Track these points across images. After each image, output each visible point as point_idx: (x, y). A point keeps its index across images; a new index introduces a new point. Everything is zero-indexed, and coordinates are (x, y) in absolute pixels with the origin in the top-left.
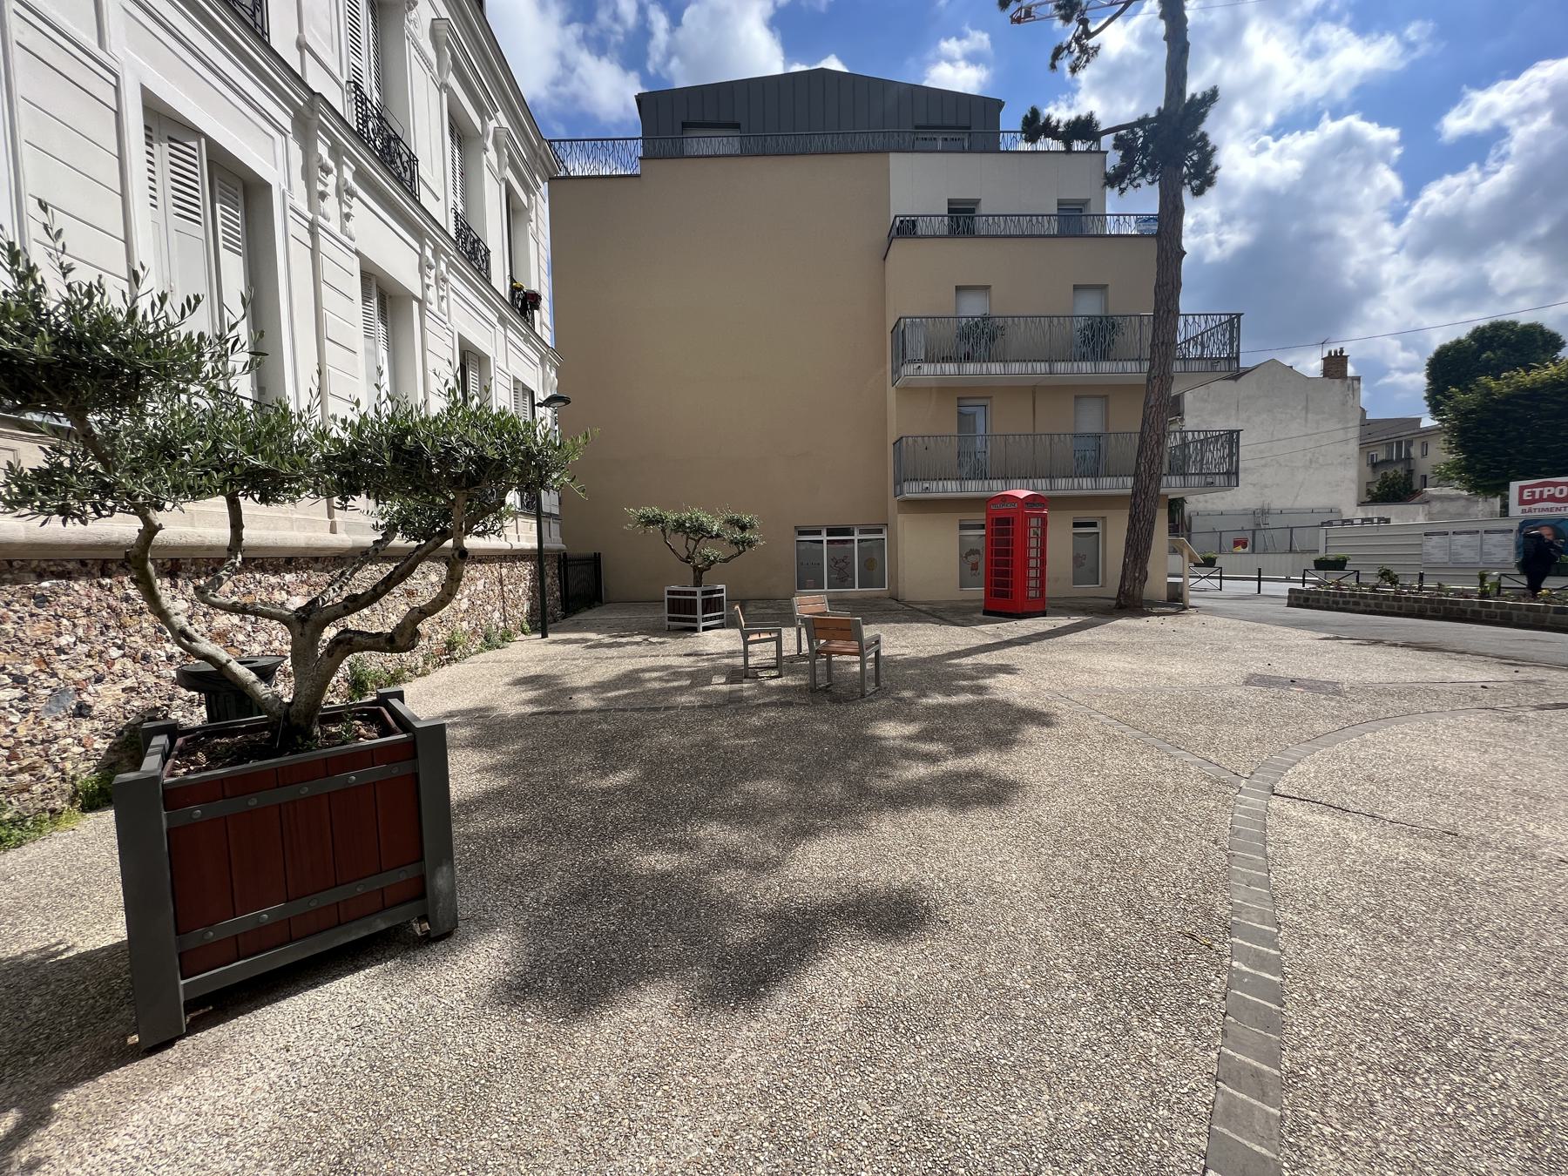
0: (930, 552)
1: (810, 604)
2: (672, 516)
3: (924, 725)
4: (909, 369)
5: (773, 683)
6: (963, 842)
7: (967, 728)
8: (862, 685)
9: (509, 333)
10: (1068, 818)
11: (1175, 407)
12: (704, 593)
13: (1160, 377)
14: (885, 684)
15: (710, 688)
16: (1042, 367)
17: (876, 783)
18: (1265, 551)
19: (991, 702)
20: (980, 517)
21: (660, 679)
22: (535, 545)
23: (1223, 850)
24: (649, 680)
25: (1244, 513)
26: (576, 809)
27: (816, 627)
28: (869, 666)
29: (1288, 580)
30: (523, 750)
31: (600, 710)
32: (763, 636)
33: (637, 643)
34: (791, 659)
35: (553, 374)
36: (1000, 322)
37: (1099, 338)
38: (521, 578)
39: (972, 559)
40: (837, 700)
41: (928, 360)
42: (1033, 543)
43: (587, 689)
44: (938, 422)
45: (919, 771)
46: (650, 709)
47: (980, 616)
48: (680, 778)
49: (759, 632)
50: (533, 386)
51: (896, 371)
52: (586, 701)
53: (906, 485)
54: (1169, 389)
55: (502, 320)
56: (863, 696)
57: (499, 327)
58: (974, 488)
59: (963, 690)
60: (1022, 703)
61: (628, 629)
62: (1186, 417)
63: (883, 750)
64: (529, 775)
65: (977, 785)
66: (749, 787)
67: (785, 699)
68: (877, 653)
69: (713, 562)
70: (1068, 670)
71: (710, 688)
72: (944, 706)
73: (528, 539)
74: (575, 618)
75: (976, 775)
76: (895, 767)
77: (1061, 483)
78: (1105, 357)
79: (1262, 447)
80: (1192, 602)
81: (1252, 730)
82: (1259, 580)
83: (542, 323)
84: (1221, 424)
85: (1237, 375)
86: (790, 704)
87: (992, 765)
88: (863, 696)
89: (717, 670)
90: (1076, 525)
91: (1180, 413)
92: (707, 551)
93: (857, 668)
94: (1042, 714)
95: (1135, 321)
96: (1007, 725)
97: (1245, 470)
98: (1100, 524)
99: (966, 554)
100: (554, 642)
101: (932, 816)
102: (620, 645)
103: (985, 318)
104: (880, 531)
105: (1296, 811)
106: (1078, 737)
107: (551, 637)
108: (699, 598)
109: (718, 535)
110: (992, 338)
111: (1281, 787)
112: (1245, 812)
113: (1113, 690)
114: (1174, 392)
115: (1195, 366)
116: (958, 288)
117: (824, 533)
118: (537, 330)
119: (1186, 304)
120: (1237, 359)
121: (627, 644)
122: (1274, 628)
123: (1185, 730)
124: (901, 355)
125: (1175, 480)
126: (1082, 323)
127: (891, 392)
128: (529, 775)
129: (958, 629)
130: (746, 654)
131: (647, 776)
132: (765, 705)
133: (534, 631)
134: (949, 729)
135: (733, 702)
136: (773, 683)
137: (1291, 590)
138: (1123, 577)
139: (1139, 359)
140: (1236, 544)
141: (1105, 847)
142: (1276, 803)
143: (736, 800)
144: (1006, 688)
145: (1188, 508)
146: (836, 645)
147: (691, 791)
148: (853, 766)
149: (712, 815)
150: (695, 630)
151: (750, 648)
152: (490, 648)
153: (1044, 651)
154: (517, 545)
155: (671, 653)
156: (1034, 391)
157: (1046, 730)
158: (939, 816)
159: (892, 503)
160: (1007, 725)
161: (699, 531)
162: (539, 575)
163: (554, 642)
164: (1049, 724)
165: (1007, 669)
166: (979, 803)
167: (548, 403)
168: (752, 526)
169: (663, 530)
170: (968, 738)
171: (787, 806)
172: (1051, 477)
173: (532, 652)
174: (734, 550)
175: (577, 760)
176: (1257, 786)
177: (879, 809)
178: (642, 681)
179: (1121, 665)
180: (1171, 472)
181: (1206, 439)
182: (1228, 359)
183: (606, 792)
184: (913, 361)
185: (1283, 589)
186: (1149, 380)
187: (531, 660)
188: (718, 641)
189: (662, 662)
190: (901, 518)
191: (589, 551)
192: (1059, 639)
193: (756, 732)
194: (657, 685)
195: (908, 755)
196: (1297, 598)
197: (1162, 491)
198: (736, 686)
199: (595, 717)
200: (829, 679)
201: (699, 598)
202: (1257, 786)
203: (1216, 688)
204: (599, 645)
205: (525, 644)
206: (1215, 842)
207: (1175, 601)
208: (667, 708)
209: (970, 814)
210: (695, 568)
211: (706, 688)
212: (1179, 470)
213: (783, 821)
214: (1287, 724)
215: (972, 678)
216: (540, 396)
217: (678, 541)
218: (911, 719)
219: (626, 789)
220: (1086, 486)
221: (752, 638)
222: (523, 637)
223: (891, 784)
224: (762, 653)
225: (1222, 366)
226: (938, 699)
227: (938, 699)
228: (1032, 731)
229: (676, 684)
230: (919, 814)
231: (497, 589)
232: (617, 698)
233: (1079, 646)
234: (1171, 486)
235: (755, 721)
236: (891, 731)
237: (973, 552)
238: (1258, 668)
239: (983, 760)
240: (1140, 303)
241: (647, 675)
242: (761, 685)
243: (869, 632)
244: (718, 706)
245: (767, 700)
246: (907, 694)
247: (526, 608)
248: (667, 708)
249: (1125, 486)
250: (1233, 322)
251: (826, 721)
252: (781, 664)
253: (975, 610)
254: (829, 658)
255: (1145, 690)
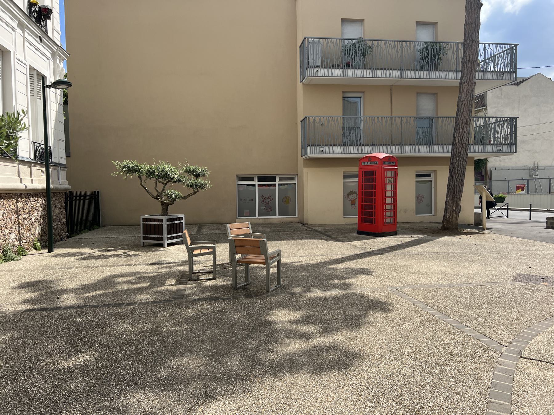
0: (324, 193)
1: (239, 229)
2: (146, 167)
3: (305, 312)
4: (311, 72)
5: (209, 283)
6: (316, 399)
7: (334, 314)
8: (267, 285)
9: (27, 35)
10: (388, 378)
11: (482, 101)
12: (168, 220)
13: (468, 82)
14: (283, 284)
15: (163, 288)
16: (396, 74)
17: (265, 357)
18: (536, 193)
19: (352, 295)
20: (355, 170)
21: (129, 282)
22: (44, 186)
23: (485, 398)
24: (120, 283)
25: (523, 169)
26: (42, 385)
27: (236, 246)
28: (273, 271)
29: (548, 211)
30: (11, 340)
31: (78, 307)
32: (203, 251)
33: (118, 256)
34: (224, 266)
35: (62, 65)
36: (369, 43)
37: (431, 56)
38: (34, 209)
39: (352, 197)
40: (249, 295)
41: (322, 66)
42: (389, 187)
43: (72, 290)
44: (333, 108)
45: (295, 346)
46: (116, 305)
47: (355, 234)
48: (126, 357)
49: (201, 248)
50: (45, 73)
51: (302, 73)
52: (70, 300)
53: (308, 149)
54: (473, 90)
55: (21, 26)
56: (268, 292)
57: (18, 30)
58: (352, 152)
59: (335, 286)
60: (372, 295)
61: (113, 245)
62: (488, 108)
63: (274, 331)
64: (12, 359)
65: (333, 356)
66: (174, 362)
67: (216, 294)
68: (278, 262)
69: (175, 200)
70: (406, 272)
71: (163, 288)
72: (319, 298)
73: (40, 182)
74: (78, 237)
75: (333, 348)
76: (279, 344)
77: (408, 149)
78: (435, 68)
79: (534, 127)
80: (488, 225)
81: (513, 313)
82: (530, 211)
83: (54, 29)
84: (508, 113)
85: (519, 83)
86: (217, 299)
87: (345, 340)
88: (268, 292)
89: (170, 275)
90: (418, 176)
91: (484, 105)
92: (169, 192)
93: (264, 273)
94: (385, 304)
95: (454, 46)
96: (359, 310)
97: (524, 142)
98: (432, 175)
99: (347, 194)
100: (58, 255)
101: (298, 380)
102: (106, 257)
103: (360, 40)
104: (293, 179)
105: (532, 368)
106: (403, 320)
107: (56, 251)
108: (165, 224)
109: (179, 181)
110: (365, 54)
111: (526, 353)
112: (502, 371)
113: (432, 286)
114: (478, 91)
115: (490, 76)
116: (343, 21)
117: (256, 179)
118: (50, 34)
119: (484, 36)
120: (515, 72)
121: (111, 256)
122: (536, 243)
123: (473, 313)
124: (306, 65)
125: (478, 148)
126: (421, 46)
127: (300, 86)
128: (12, 359)
129: (339, 244)
130: (191, 263)
131: (102, 358)
132: (199, 300)
133: (43, 247)
134: (322, 317)
135: (178, 298)
136: (209, 283)
137: (548, 218)
138: (446, 210)
139: (456, 71)
140: (518, 188)
141: (410, 400)
142: (522, 363)
143: (164, 372)
144: (364, 286)
145: (490, 165)
146: (251, 257)
147: (132, 367)
148: (251, 344)
149: (142, 386)
150: (162, 246)
151: (195, 259)
152: (6, 260)
153: (392, 259)
154: (30, 186)
155: (142, 262)
156: (392, 89)
157: (384, 315)
158: (303, 379)
159: (300, 160)
160: (359, 310)
161: (165, 178)
162: (48, 208)
163: (58, 255)
164: (386, 310)
165: (366, 272)
166: (331, 369)
167: (56, 84)
168: (203, 175)
169: (140, 177)
170: (332, 321)
171: (198, 377)
172: (401, 145)
173: (38, 264)
174: (191, 191)
175: (51, 346)
176: (512, 352)
177: (262, 376)
178: (115, 284)
179: (439, 268)
180: (476, 143)
181: (497, 122)
182: (510, 72)
183: (67, 371)
184: (314, 67)
185: (543, 217)
186: (461, 84)
187: (36, 269)
188: (175, 254)
189: (133, 269)
190: (306, 170)
191: (89, 189)
192: (403, 251)
193: (189, 320)
194: (125, 287)
195: (291, 334)
196: (551, 223)
197: (470, 155)
198: (182, 287)
199: (73, 312)
200: (247, 280)
201: (165, 224)
202: (512, 352)
203: (496, 284)
204: (91, 257)
205: (34, 257)
206: (481, 394)
207: (478, 225)
208: (128, 304)
209: (324, 378)
210: (163, 203)
211: (160, 289)
212: (482, 141)
213: (193, 389)
214: (536, 308)
215: (342, 278)
216: (50, 80)
217: (150, 184)
218: (297, 308)
219: (82, 368)
220: (423, 151)
221: (196, 252)
222: (35, 251)
223: (274, 357)
224: (204, 262)
225: (506, 76)
226: (318, 293)
227: (318, 293)
228: (375, 315)
229: (139, 286)
230: (289, 379)
231: (14, 217)
232: (93, 297)
233: (415, 256)
234: (476, 152)
235: (190, 312)
236: (282, 317)
237: (352, 193)
238: (523, 270)
239: (341, 338)
240: (458, 36)
241: (120, 280)
242: (200, 285)
243: (272, 247)
244: (166, 301)
245: (202, 296)
246: (298, 290)
247: (37, 230)
248: (128, 304)
249: (446, 151)
250: (513, 49)
251: (239, 311)
252: (216, 271)
253: (351, 231)
254: (247, 267)
255: (451, 286)
